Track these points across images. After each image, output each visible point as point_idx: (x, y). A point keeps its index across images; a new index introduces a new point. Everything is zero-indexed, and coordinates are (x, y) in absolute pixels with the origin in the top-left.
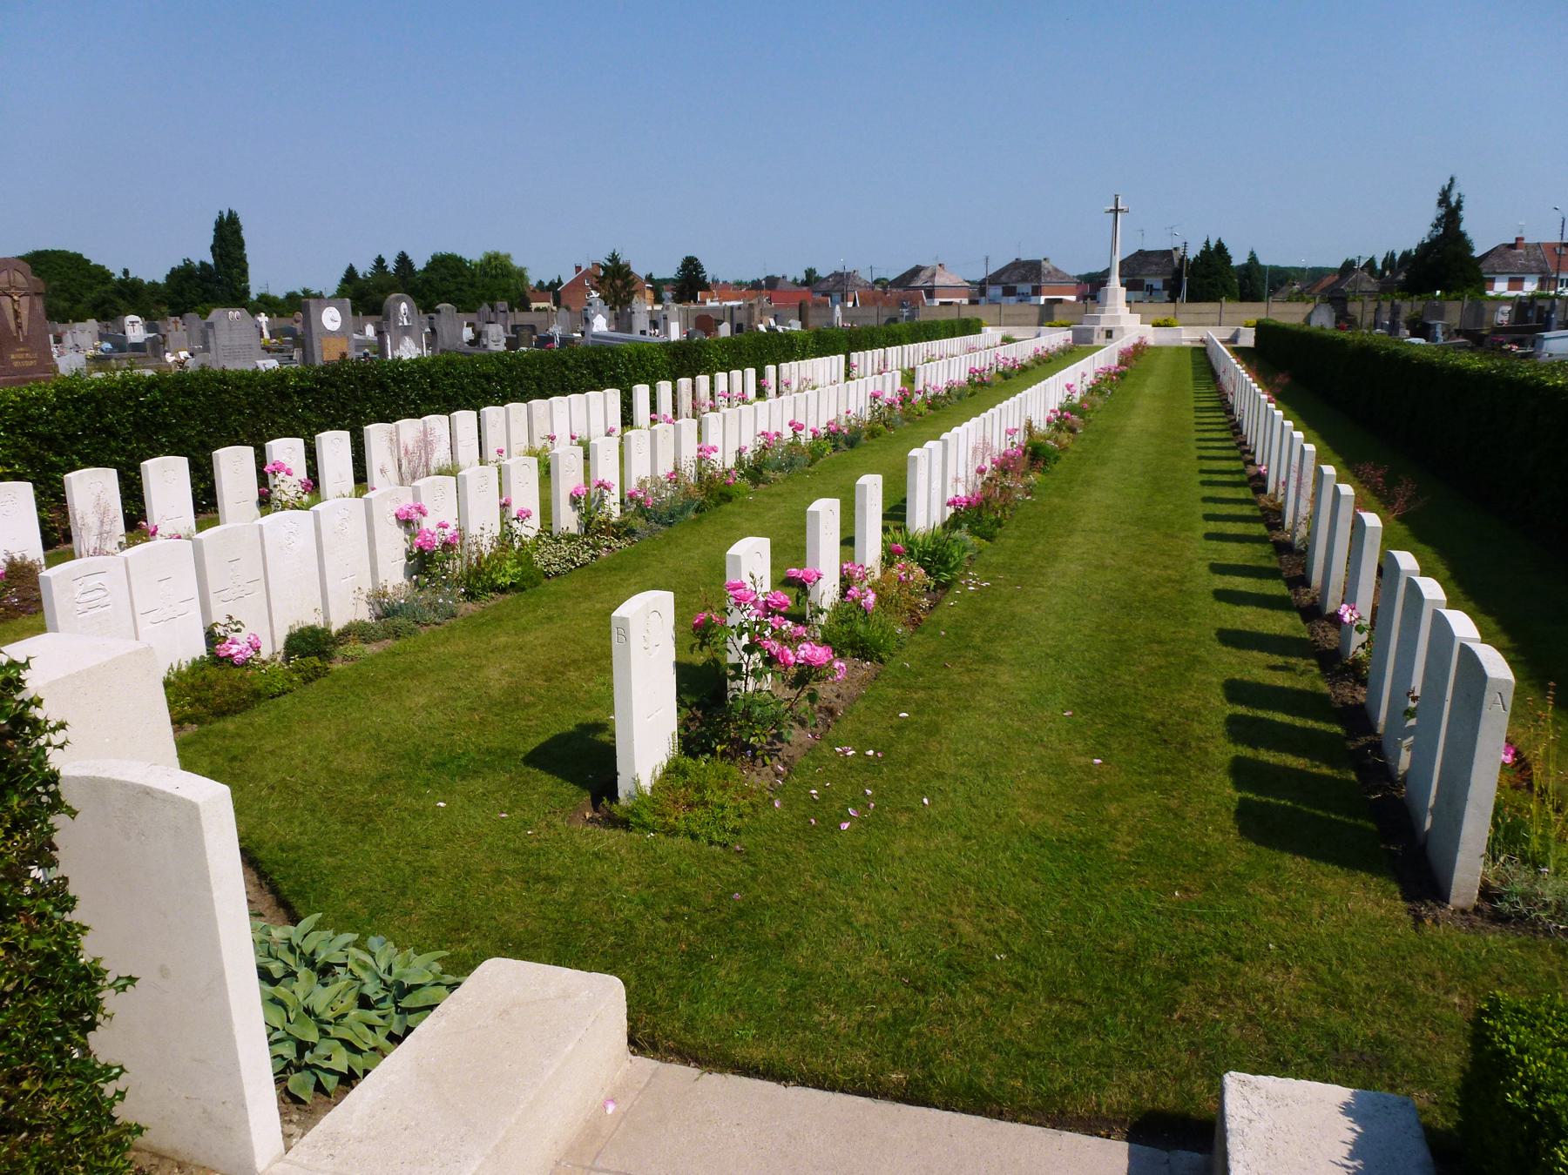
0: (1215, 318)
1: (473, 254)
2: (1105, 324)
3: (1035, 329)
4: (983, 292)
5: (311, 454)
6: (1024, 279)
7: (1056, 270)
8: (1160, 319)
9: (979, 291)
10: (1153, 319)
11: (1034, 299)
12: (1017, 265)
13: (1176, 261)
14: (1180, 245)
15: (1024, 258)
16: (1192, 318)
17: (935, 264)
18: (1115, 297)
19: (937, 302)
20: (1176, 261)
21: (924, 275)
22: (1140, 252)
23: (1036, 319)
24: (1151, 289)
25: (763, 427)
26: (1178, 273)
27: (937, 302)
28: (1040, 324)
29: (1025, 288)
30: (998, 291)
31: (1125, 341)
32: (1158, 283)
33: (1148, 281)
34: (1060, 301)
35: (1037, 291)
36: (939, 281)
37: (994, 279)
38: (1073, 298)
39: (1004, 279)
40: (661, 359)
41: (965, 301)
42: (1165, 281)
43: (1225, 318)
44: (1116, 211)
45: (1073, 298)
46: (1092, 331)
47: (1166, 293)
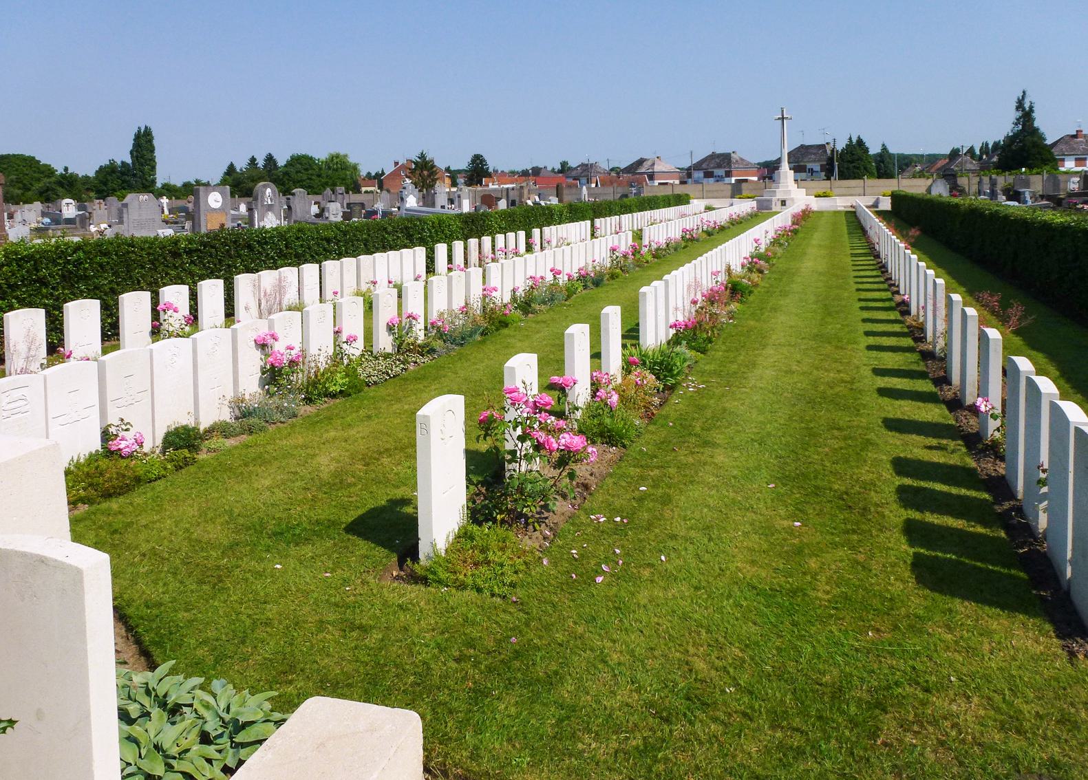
2: (780, 195)
3: (729, 201)
4: (689, 175)
6: (719, 166)
7: (742, 159)
8: (820, 192)
11: (727, 180)
12: (713, 156)
15: (718, 152)
16: (843, 191)
19: (656, 183)
20: (829, 152)
21: (646, 165)
23: (729, 193)
24: (812, 171)
26: (831, 160)
28: (732, 197)
29: (720, 172)
32: (817, 167)
33: (809, 166)
35: (729, 174)
36: (657, 168)
37: (697, 166)
38: (755, 179)
39: (704, 166)
41: (677, 182)
42: (821, 166)
43: (868, 190)
45: (755, 179)
46: (770, 201)
47: (823, 173)
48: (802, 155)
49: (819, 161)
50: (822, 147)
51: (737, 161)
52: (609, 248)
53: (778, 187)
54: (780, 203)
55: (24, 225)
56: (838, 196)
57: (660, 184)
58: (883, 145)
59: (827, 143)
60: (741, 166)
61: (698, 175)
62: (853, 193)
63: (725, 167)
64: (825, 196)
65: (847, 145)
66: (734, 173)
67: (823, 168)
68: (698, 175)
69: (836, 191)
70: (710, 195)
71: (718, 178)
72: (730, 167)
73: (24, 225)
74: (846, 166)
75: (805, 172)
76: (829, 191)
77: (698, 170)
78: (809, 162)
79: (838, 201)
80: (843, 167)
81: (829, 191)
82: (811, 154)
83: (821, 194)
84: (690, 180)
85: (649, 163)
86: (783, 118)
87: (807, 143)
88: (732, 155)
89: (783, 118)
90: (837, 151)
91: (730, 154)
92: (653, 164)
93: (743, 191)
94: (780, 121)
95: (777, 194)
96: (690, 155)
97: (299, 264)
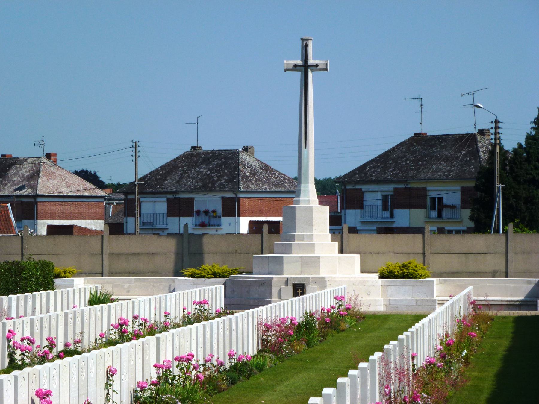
0: (498, 263)
1: (85, 169)
2: (292, 272)
4: (130, 209)
6: (207, 186)
7: (266, 168)
8: (394, 263)
9: (125, 204)
10: (382, 267)
12: (195, 157)
15: (207, 146)
16: (455, 262)
17: (40, 153)
19: (42, 226)
20: (484, 155)
21: (18, 175)
22: (419, 139)
23: (170, 263)
24: (439, 205)
25: (332, 305)
26: (486, 177)
27: (42, 226)
28: (178, 273)
29: (210, 201)
30: (161, 206)
31: (317, 302)
32: (452, 196)
33: (434, 190)
34: (68, 230)
35: (232, 209)
36: (46, 185)
37: (151, 184)
38: (98, 225)
39: (170, 183)
40: (454, 232)
42: (464, 191)
43: (515, 262)
45: (98, 225)
46: (268, 284)
47: (466, 213)
48: (416, 161)
49: (458, 178)
51: (253, 173)
53: (288, 250)
54: (290, 289)
56: (436, 275)
57: (53, 230)
59: (482, 132)
60: (266, 187)
61: (154, 207)
62: (482, 268)
63: (222, 189)
64: (405, 274)
65: (529, 138)
66: (245, 204)
68: (154, 207)
70: (123, 264)
71: (203, 218)
72: (235, 188)
75: (425, 207)
76: (417, 262)
77: (155, 193)
78: (430, 180)
81: (417, 262)
83: (396, 271)
84: (131, 220)
85: (25, 170)
86: (305, 68)
87: (431, 130)
88: (243, 156)
89: (305, 68)
90: (504, 153)
91: (235, 154)
92: (35, 175)
93: (207, 258)
94: (298, 75)
95: (286, 267)
96: (130, 152)
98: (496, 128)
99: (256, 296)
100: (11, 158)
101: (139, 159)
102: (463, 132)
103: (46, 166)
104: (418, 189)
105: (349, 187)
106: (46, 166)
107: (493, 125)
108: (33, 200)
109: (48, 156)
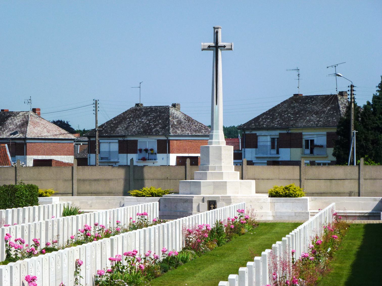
0: (352, 186)
2: (207, 192)
3: (119, 198)
4: (92, 148)
5: (49, 285)
6: (147, 132)
7: (189, 119)
8: (280, 186)
11: (161, 158)
12: (138, 111)
13: (343, 110)
14: (345, 88)
16: (322, 186)
17: (28, 108)
18: (219, 158)
19: (30, 160)
20: (343, 110)
21: (12, 124)
22: (297, 98)
23: (120, 186)
24: (311, 145)
26: (344, 125)
27: (30, 160)
28: (126, 193)
29: (149, 142)
31: (225, 214)
32: (320, 138)
33: (307, 135)
35: (164, 147)
36: (32, 131)
37: (107, 130)
39: (120, 130)
41: (70, 159)
42: (329, 135)
43: (366, 185)
44: (216, 48)
46: (190, 201)
47: (331, 151)
48: (295, 114)
49: (324, 126)
50: (331, 100)
51: (180, 122)
52: (97, 270)
53: (204, 177)
54: (206, 205)
55: (254, 284)
57: (37, 163)
58: (132, 158)
59: (341, 94)
60: (188, 132)
61: (109, 146)
62: (342, 190)
63: (157, 134)
64: (287, 194)
66: (174, 144)
67: (332, 140)
68: (109, 146)
69: (310, 185)
70: (86, 187)
71: (144, 155)
72: (167, 133)
73: (254, 284)
74: (371, 137)
75: (301, 147)
76: (295, 185)
77: (110, 137)
78: (305, 127)
79: (309, 204)
80: (366, 139)
82: (311, 112)
83: (281, 191)
84: (93, 156)
85: (18, 121)
87: (305, 93)
88: (172, 110)
89: (216, 48)
91: (166, 109)
92: (25, 124)
95: (202, 189)
96: (92, 108)
97: (127, 154)
98: (352, 90)
99: (182, 210)
100: (8, 112)
101: (98, 113)
102: (328, 93)
103: (33, 118)
104: (296, 134)
105: (247, 132)
106: (33, 118)
107: (350, 89)
108: (23, 142)
109: (34, 110)
